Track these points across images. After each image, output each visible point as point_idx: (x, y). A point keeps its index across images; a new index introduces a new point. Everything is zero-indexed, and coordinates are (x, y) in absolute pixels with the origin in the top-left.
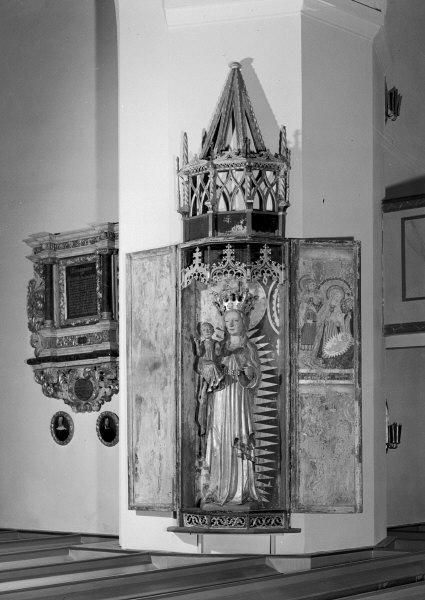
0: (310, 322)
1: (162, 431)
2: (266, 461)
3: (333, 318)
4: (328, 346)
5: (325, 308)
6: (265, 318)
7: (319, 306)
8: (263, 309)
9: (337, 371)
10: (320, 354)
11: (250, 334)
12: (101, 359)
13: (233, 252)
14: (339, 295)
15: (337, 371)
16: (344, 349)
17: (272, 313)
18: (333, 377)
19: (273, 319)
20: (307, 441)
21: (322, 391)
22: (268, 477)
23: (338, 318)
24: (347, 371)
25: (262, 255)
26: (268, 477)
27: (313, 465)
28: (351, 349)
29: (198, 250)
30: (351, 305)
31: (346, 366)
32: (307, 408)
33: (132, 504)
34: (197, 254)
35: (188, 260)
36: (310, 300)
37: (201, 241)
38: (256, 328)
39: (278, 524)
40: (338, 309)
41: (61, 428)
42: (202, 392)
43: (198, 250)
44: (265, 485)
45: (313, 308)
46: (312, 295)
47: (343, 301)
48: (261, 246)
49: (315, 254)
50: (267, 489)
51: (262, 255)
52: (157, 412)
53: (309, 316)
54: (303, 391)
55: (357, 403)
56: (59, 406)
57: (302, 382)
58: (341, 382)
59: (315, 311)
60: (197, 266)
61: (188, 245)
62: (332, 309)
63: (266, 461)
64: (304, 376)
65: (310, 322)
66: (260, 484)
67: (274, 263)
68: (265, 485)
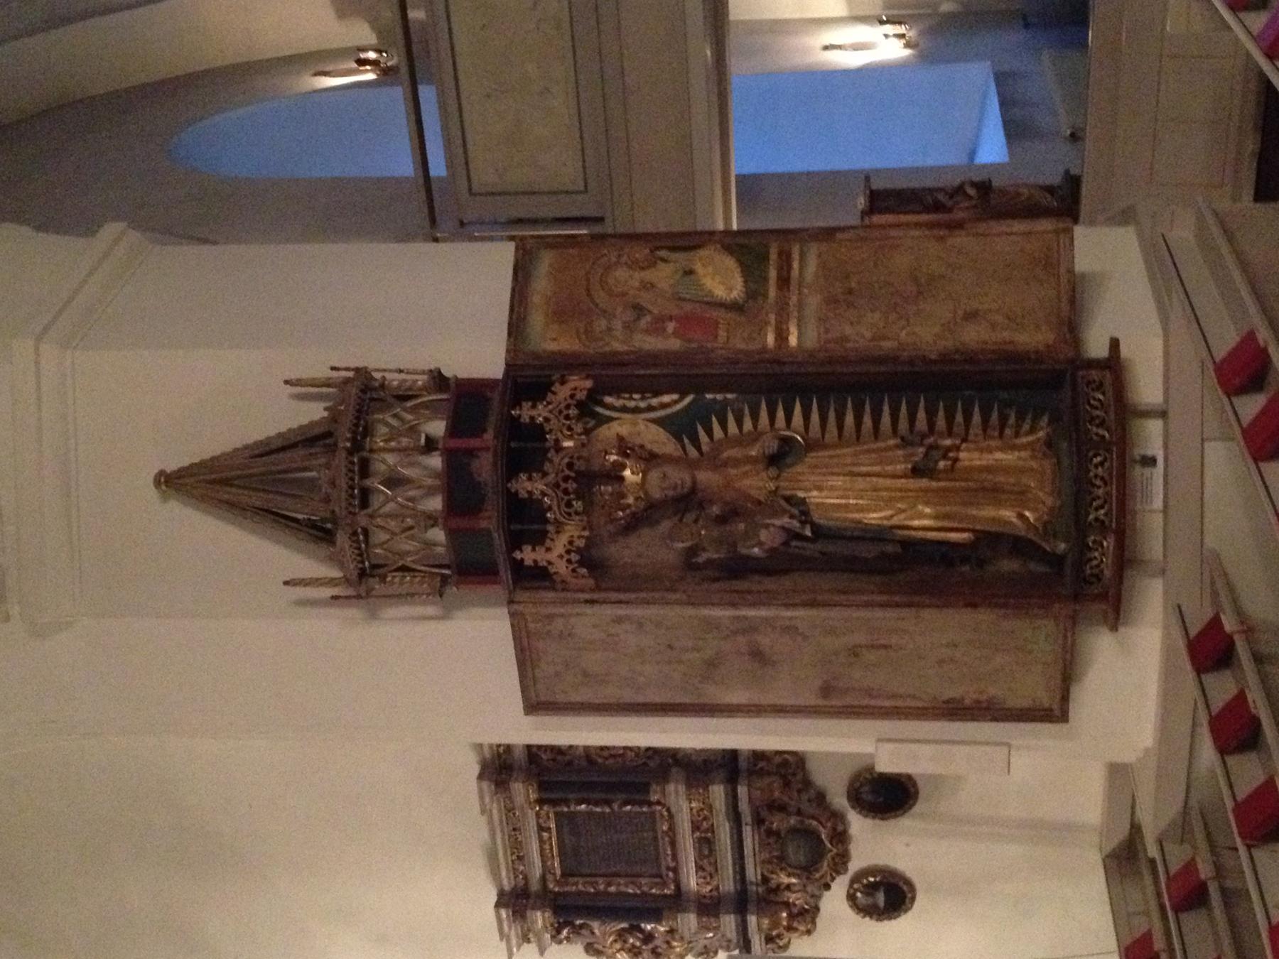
0: (671, 327)
1: (894, 640)
2: (959, 418)
3: (663, 285)
4: (720, 292)
5: (645, 299)
6: (659, 422)
7: (639, 310)
8: (642, 427)
9: (773, 274)
10: (734, 307)
11: (693, 453)
12: (744, 806)
13: (526, 405)
14: (621, 273)
15: (773, 274)
16: (730, 262)
17: (650, 409)
18: (784, 282)
19: (664, 406)
20: (917, 330)
21: (814, 302)
22: (995, 415)
23: (664, 275)
24: (773, 256)
25: (532, 418)
26: (995, 415)
27: (971, 316)
28: (728, 249)
29: (518, 555)
30: (641, 252)
31: (765, 258)
32: (848, 330)
33: (1057, 712)
34: (528, 555)
35: (539, 576)
36: (627, 326)
37: (499, 540)
38: (680, 440)
39: (1101, 384)
40: (648, 275)
41: (881, 898)
42: (812, 549)
43: (518, 555)
44: (1012, 420)
45: (645, 321)
46: (618, 325)
47: (635, 265)
48: (512, 497)
49: (536, 319)
50: (1021, 418)
51: (532, 418)
52: (854, 652)
53: (657, 327)
54: (812, 341)
55: (839, 236)
56: (835, 901)
57: (793, 341)
58: (796, 265)
59: (648, 318)
60: (553, 556)
61: (505, 574)
62: (648, 286)
63: (959, 418)
64: (782, 336)
65: (671, 327)
66: (1008, 432)
67: (550, 397)
68: (1012, 420)
